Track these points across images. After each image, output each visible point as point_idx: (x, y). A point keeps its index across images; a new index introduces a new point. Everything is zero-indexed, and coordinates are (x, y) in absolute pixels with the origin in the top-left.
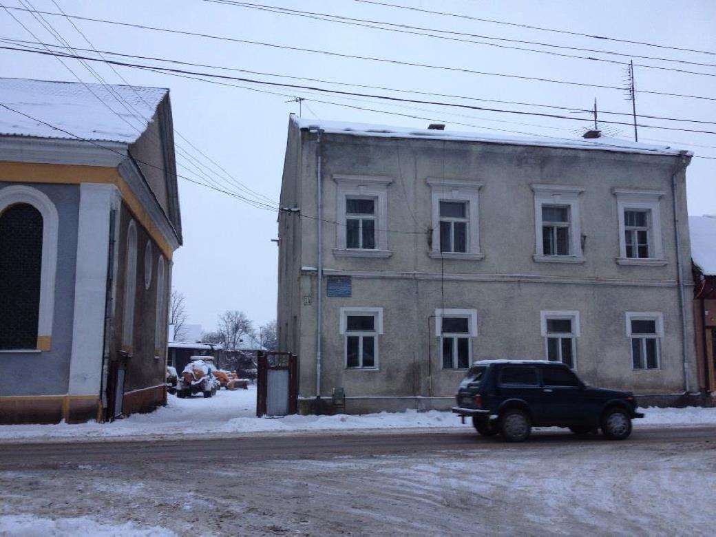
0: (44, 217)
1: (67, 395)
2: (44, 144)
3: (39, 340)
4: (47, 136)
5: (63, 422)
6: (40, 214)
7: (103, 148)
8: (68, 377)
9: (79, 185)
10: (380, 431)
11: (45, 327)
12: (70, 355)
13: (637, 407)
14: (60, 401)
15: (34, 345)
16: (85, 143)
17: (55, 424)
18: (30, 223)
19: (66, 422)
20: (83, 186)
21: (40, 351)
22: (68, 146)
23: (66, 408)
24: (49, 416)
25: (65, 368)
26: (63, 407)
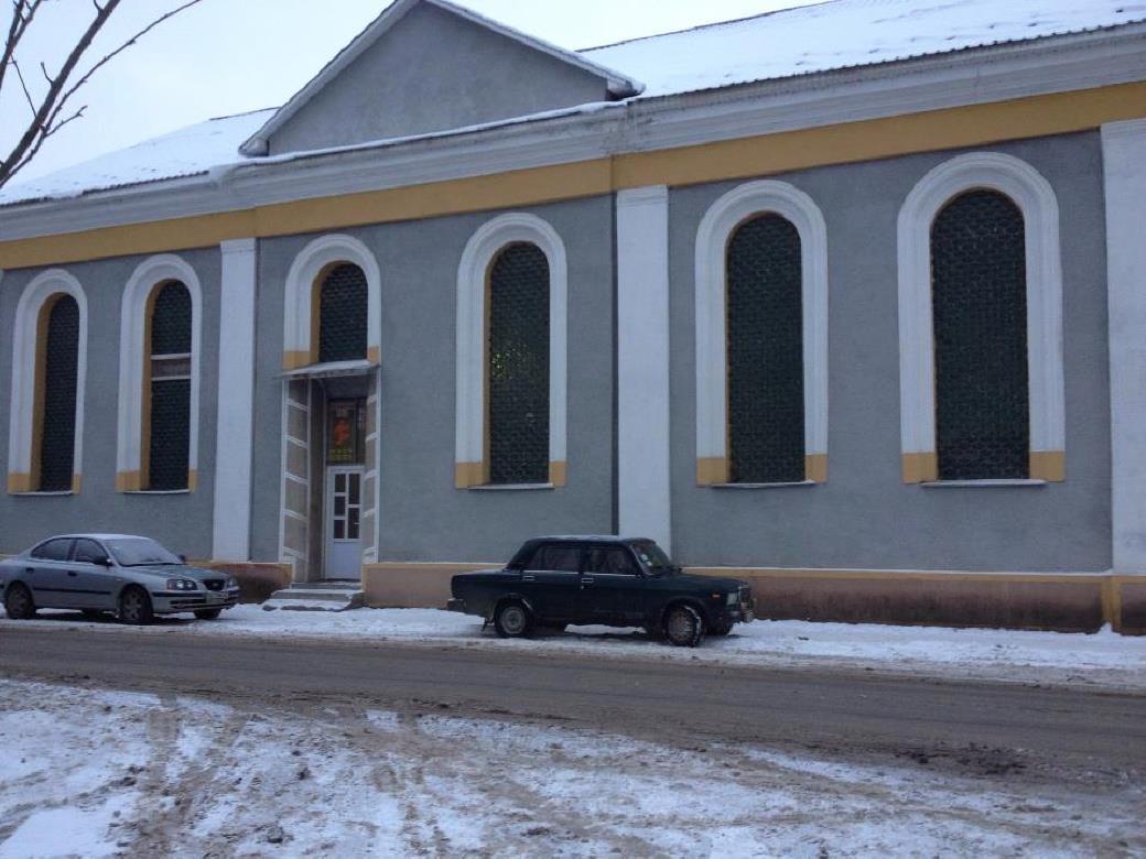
0: (548, 254)
1: (1109, 573)
2: (1038, 54)
3: (807, 459)
4: (790, 74)
5: (1107, 629)
6: (794, 230)
7: (1055, 51)
8: (1109, 537)
9: (1098, 129)
10: (812, 661)
11: (1047, 428)
12: (1109, 490)
13: (731, 626)
14: (1095, 585)
15: (545, 479)
16: (1118, 33)
17: (1088, 633)
18: (994, 226)
19: (1114, 630)
20: (1105, 128)
21: (812, 482)
22: (119, 200)
23: (1113, 601)
24: (1078, 617)
25: (1102, 519)
26: (1103, 597)
